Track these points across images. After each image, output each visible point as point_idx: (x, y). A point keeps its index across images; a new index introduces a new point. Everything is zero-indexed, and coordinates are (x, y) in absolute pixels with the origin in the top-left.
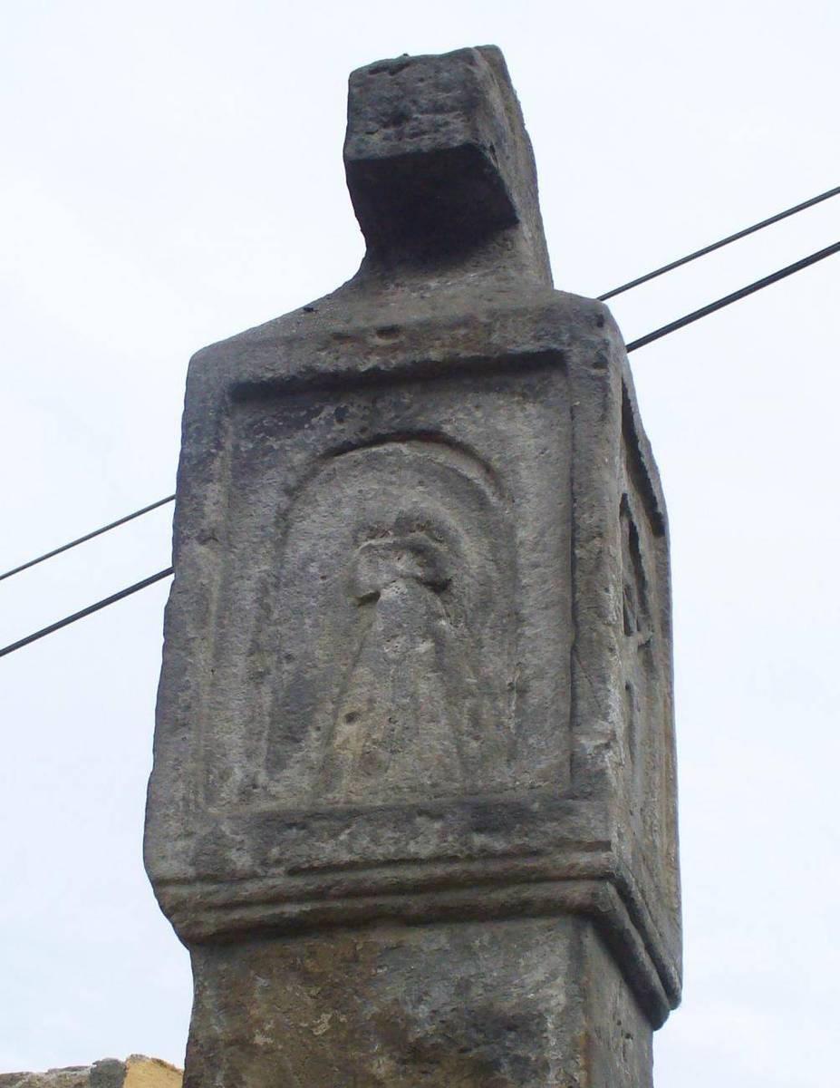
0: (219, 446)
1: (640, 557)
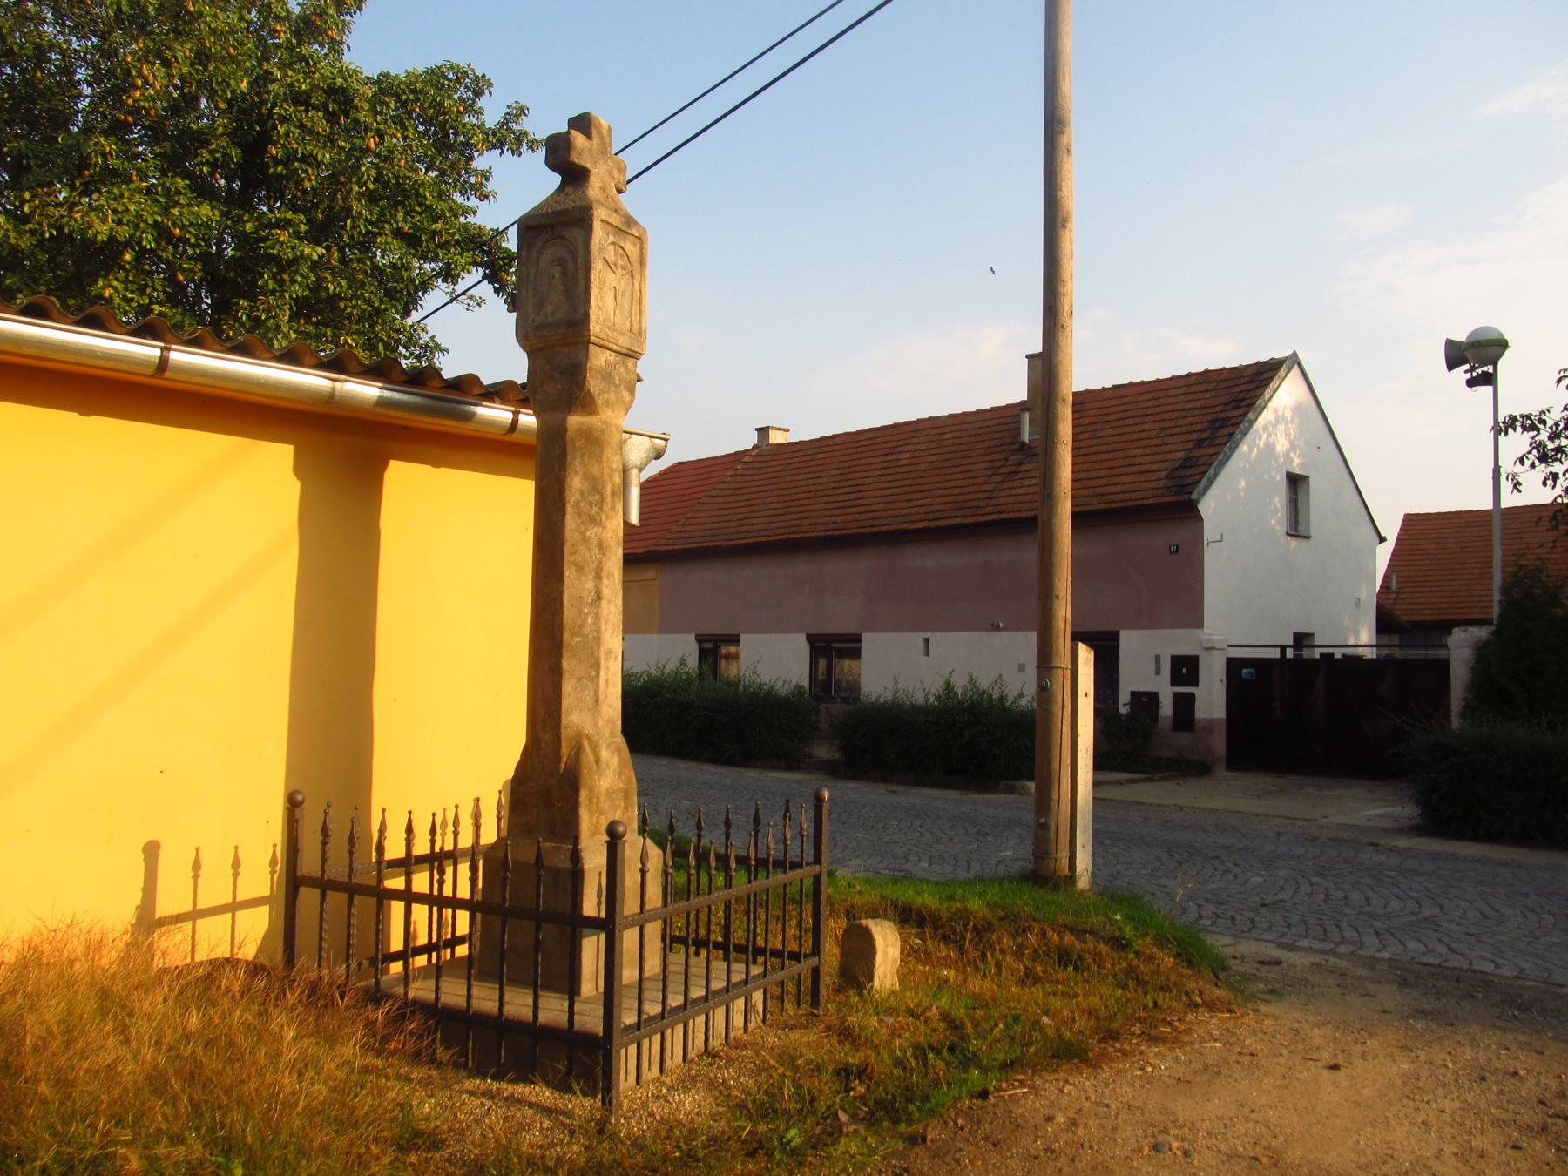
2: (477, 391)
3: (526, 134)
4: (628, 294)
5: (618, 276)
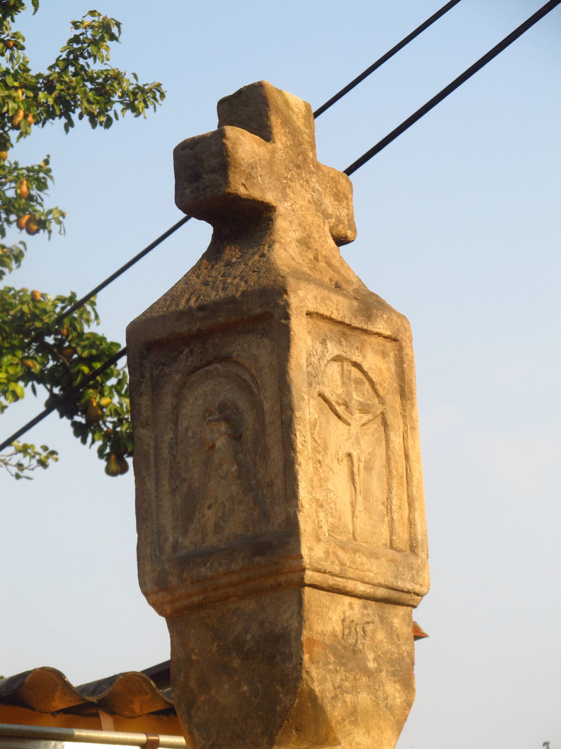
0: (143, 377)
1: (366, 372)
2: (59, 704)
3: (117, 77)
4: (379, 464)
5: (354, 428)
